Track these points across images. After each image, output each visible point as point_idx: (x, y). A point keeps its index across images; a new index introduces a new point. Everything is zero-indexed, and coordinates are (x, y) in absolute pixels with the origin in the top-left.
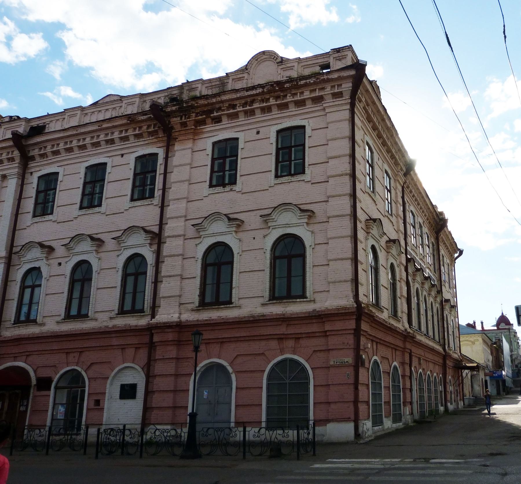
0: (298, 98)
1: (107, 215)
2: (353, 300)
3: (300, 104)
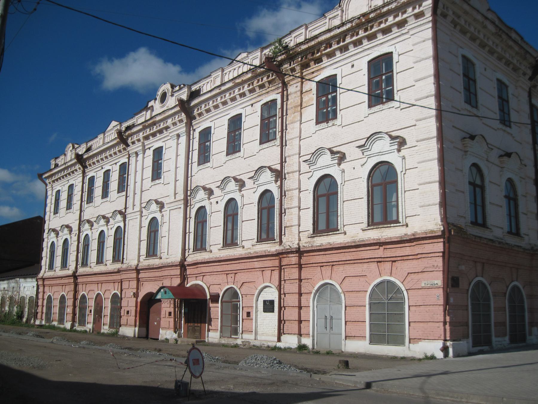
0: (383, 26)
1: (401, 109)
2: (440, 223)
3: (386, 31)
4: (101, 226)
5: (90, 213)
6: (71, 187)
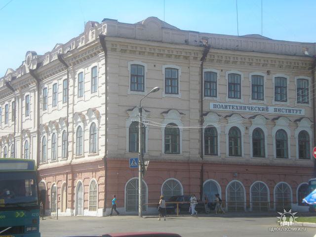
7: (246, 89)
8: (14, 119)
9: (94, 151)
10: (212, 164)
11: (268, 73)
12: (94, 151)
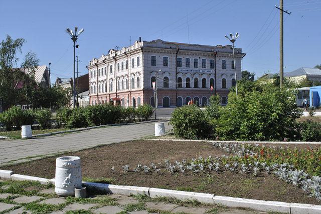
4: (122, 78)
5: (119, 74)
6: (138, 58)
7: (192, 64)
8: (106, 74)
9: (138, 86)
10: (181, 90)
11: (200, 58)
12: (138, 86)
